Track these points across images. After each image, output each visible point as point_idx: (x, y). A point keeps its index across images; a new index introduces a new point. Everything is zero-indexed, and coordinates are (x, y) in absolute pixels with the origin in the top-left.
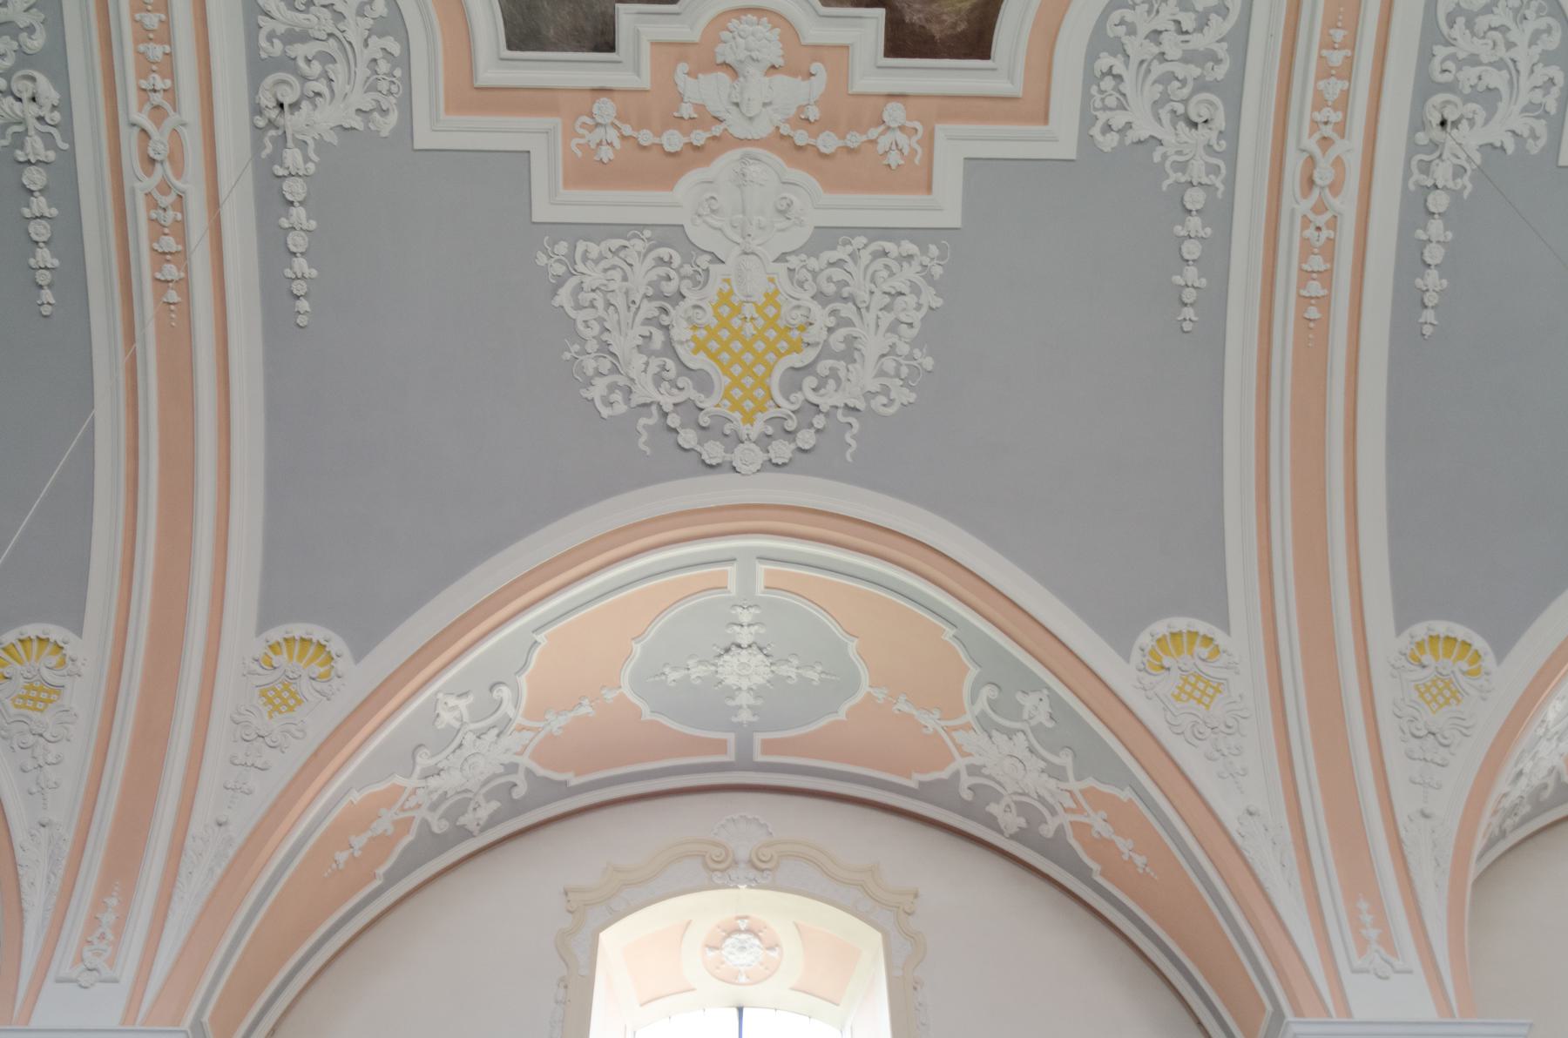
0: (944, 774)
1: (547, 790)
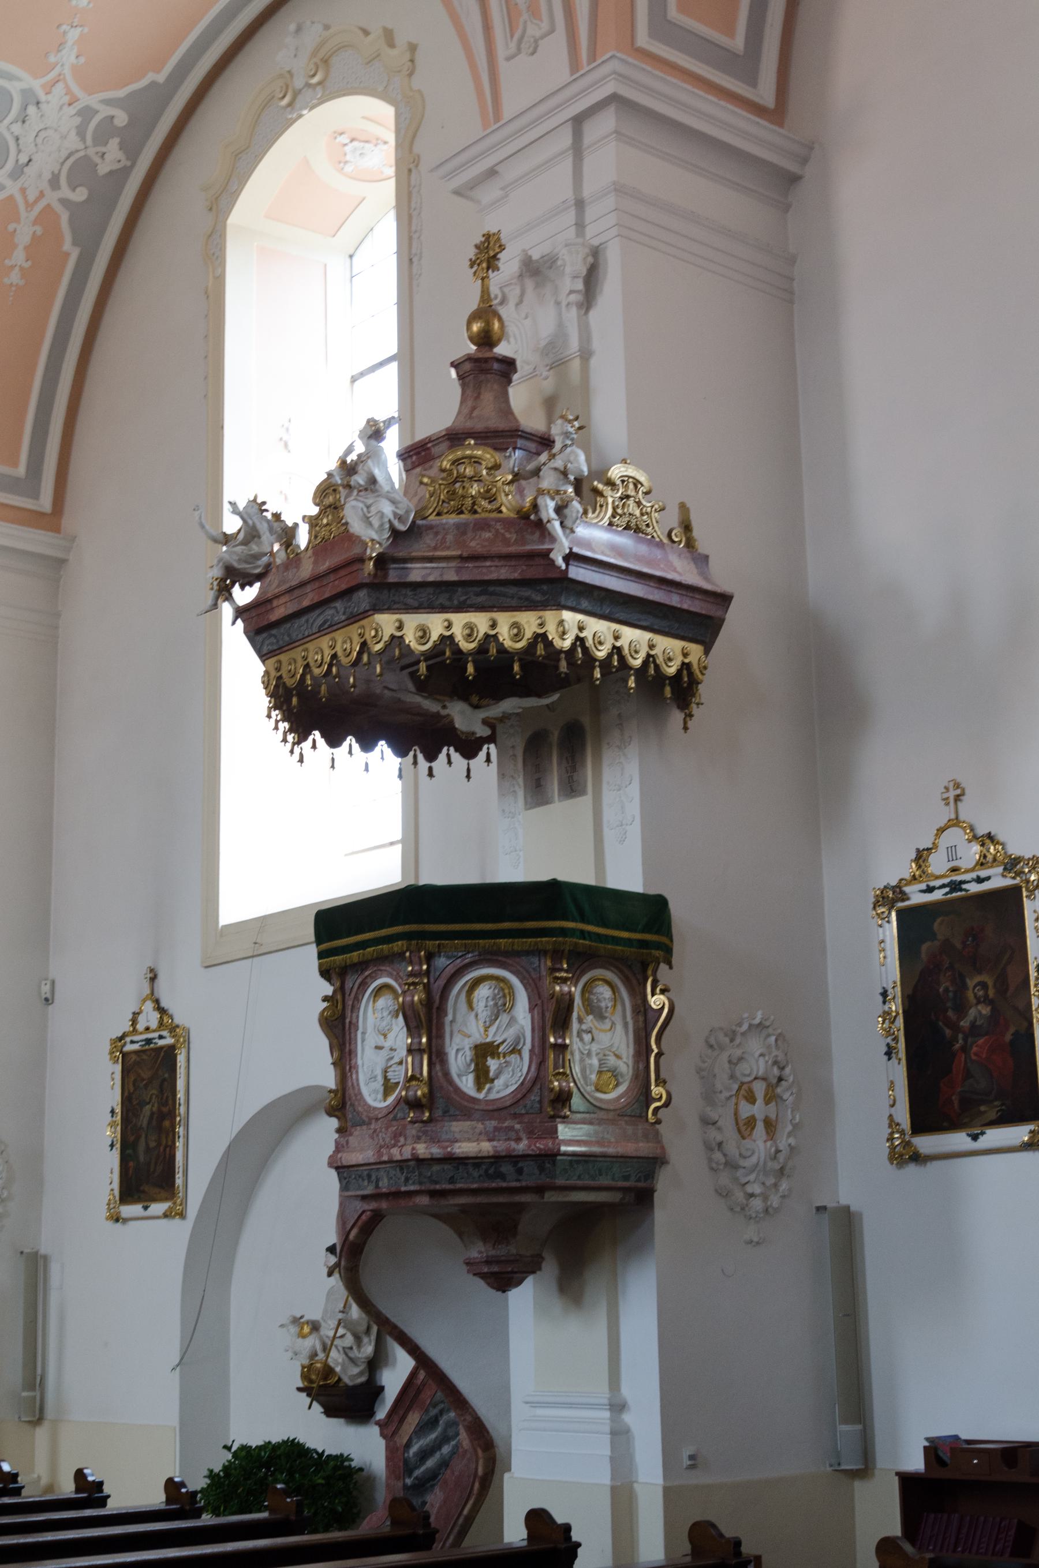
0: (64, 217)
1: (144, 106)
